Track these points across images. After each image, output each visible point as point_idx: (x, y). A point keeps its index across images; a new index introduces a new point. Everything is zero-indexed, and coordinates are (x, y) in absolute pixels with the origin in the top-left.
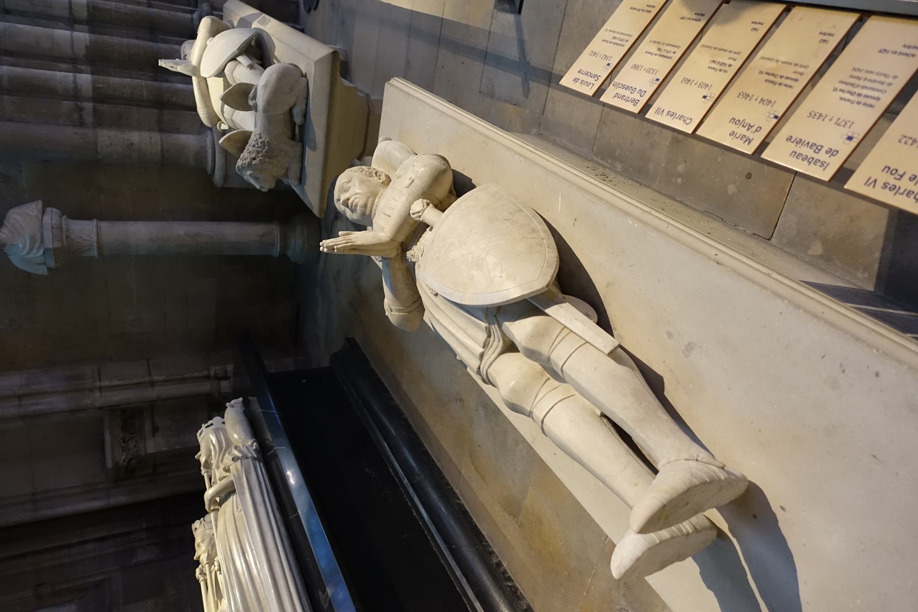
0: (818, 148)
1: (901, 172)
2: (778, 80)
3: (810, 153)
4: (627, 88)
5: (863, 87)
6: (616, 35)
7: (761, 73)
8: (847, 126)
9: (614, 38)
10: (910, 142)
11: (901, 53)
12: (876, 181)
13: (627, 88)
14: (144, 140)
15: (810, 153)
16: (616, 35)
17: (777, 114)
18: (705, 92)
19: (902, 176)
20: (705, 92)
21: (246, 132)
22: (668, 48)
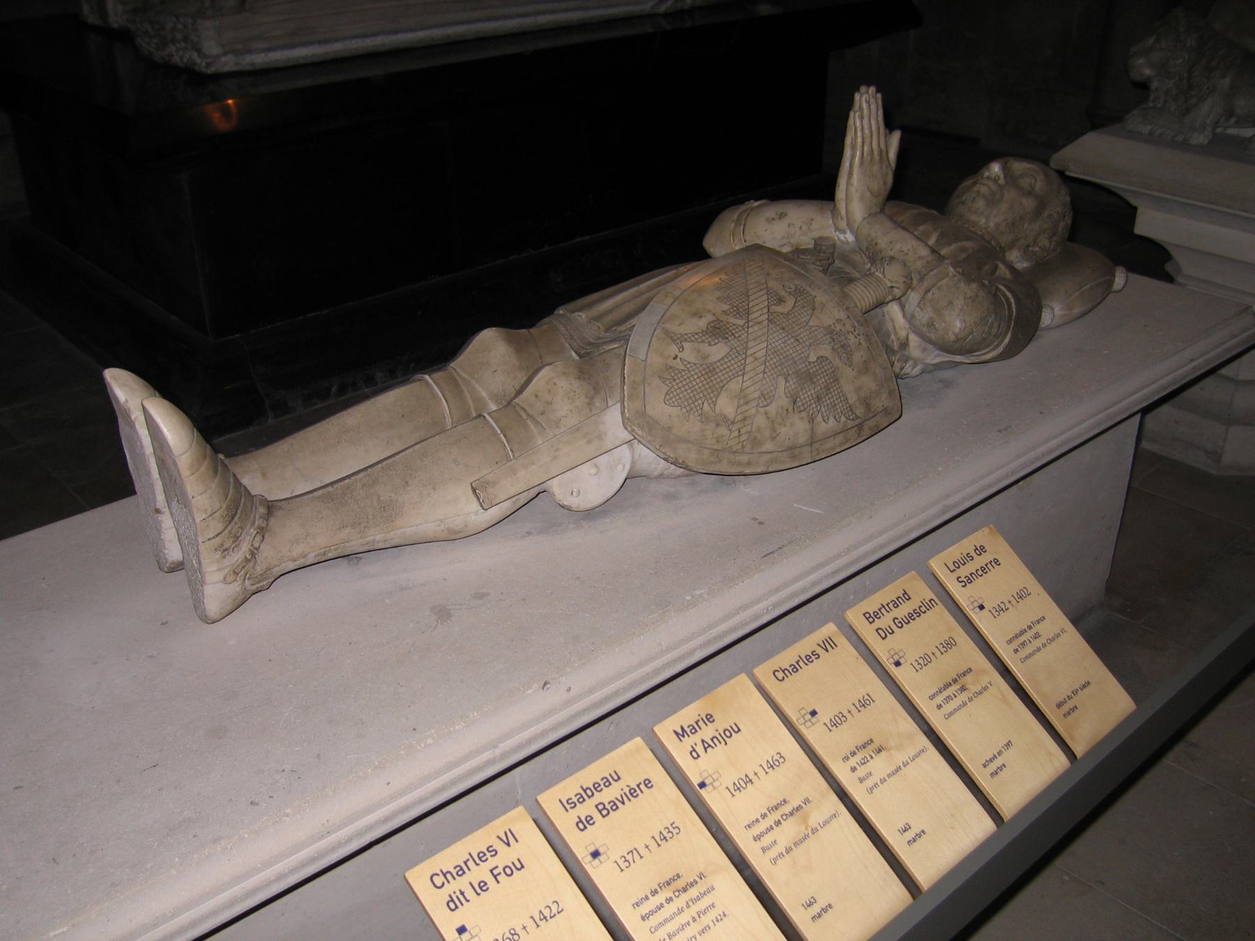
0: (603, 810)
1: (502, 878)
2: (776, 816)
3: (606, 796)
4: (911, 617)
5: (680, 911)
6: (1038, 643)
7: (807, 801)
8: (621, 862)
9: (1037, 636)
10: (547, 912)
11: (1000, 753)
12: (508, 844)
13: (911, 617)
14: (334, 389)
15: (606, 796)
16: (1038, 643)
17: (709, 788)
18: (824, 716)
19: (495, 877)
20: (824, 716)
21: (910, 212)
22: (1029, 649)
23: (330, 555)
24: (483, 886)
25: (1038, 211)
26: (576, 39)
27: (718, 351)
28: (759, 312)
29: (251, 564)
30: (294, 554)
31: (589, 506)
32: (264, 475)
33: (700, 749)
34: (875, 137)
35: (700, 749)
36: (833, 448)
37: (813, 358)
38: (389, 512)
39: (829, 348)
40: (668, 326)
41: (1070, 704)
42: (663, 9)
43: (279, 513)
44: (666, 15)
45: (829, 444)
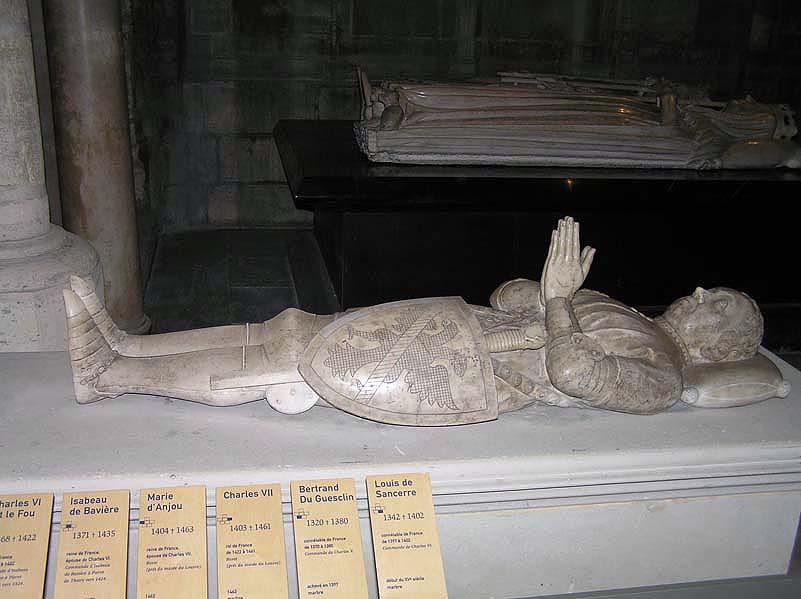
23: (142, 391)
24: (12, 515)
25: (721, 326)
26: (486, 175)
27: (374, 345)
28: (413, 332)
29: (96, 380)
30: (121, 383)
31: (293, 412)
32: (141, 348)
33: (154, 508)
34: (569, 250)
35: (154, 508)
36: (434, 422)
37: (434, 365)
38: (172, 377)
39: (449, 363)
40: (353, 324)
41: (398, 584)
42: (697, 166)
43: (120, 362)
44: (698, 171)
45: (431, 418)
